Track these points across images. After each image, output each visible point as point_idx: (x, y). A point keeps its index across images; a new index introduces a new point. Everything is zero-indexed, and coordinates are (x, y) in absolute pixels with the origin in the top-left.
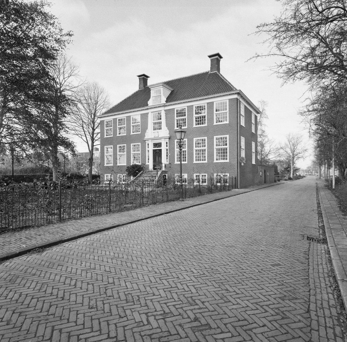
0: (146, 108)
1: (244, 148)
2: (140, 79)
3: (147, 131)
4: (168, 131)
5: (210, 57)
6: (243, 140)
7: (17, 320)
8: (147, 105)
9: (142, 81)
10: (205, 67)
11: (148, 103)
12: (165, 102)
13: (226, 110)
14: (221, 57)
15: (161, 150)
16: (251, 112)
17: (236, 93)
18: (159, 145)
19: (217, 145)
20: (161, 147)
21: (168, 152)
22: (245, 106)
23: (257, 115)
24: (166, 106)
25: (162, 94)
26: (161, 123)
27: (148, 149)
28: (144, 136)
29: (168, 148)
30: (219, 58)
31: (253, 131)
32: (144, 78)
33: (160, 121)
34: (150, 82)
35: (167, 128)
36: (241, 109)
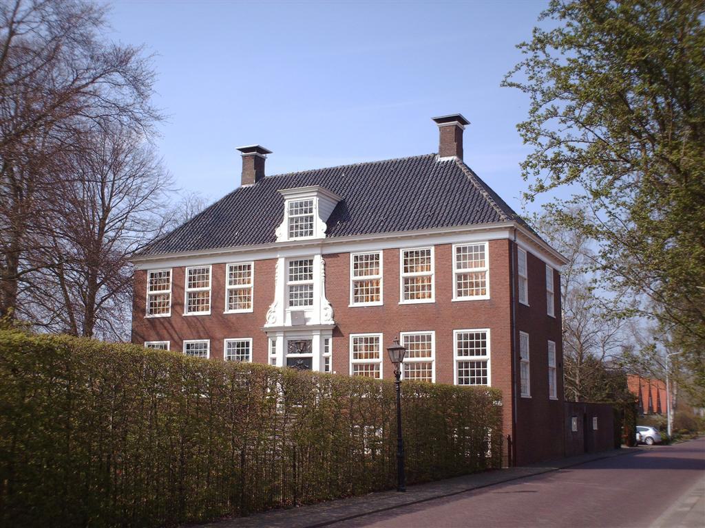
0: (272, 246)
1: (528, 360)
2: (244, 157)
3: (272, 307)
4: (330, 311)
5: (439, 120)
6: (525, 337)
7: (519, 492)
8: (275, 238)
9: (252, 163)
10: (424, 142)
11: (277, 233)
12: (324, 236)
13: (429, 269)
14: (464, 122)
15: (310, 359)
16: (544, 264)
17: (506, 228)
18: (305, 346)
19: (460, 353)
20: (311, 352)
21: (330, 365)
22: (528, 253)
23: (558, 268)
24: (328, 245)
25: (315, 213)
26: (291, 277)
27: (273, 356)
28: (264, 321)
29: (330, 354)
30: (460, 125)
31: (552, 313)
32: (256, 157)
33: (308, 282)
34: (270, 170)
35: (327, 302)
36: (520, 262)
